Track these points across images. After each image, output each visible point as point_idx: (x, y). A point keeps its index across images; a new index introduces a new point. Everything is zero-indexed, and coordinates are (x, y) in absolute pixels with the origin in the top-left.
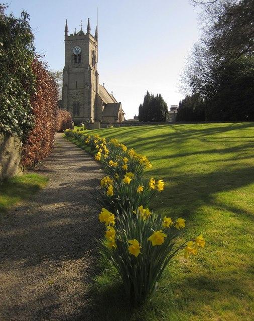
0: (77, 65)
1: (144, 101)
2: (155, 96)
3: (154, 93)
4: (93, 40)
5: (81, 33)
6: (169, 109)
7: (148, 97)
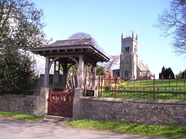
1: (162, 71)
3: (167, 67)
4: (136, 40)
7: (163, 68)
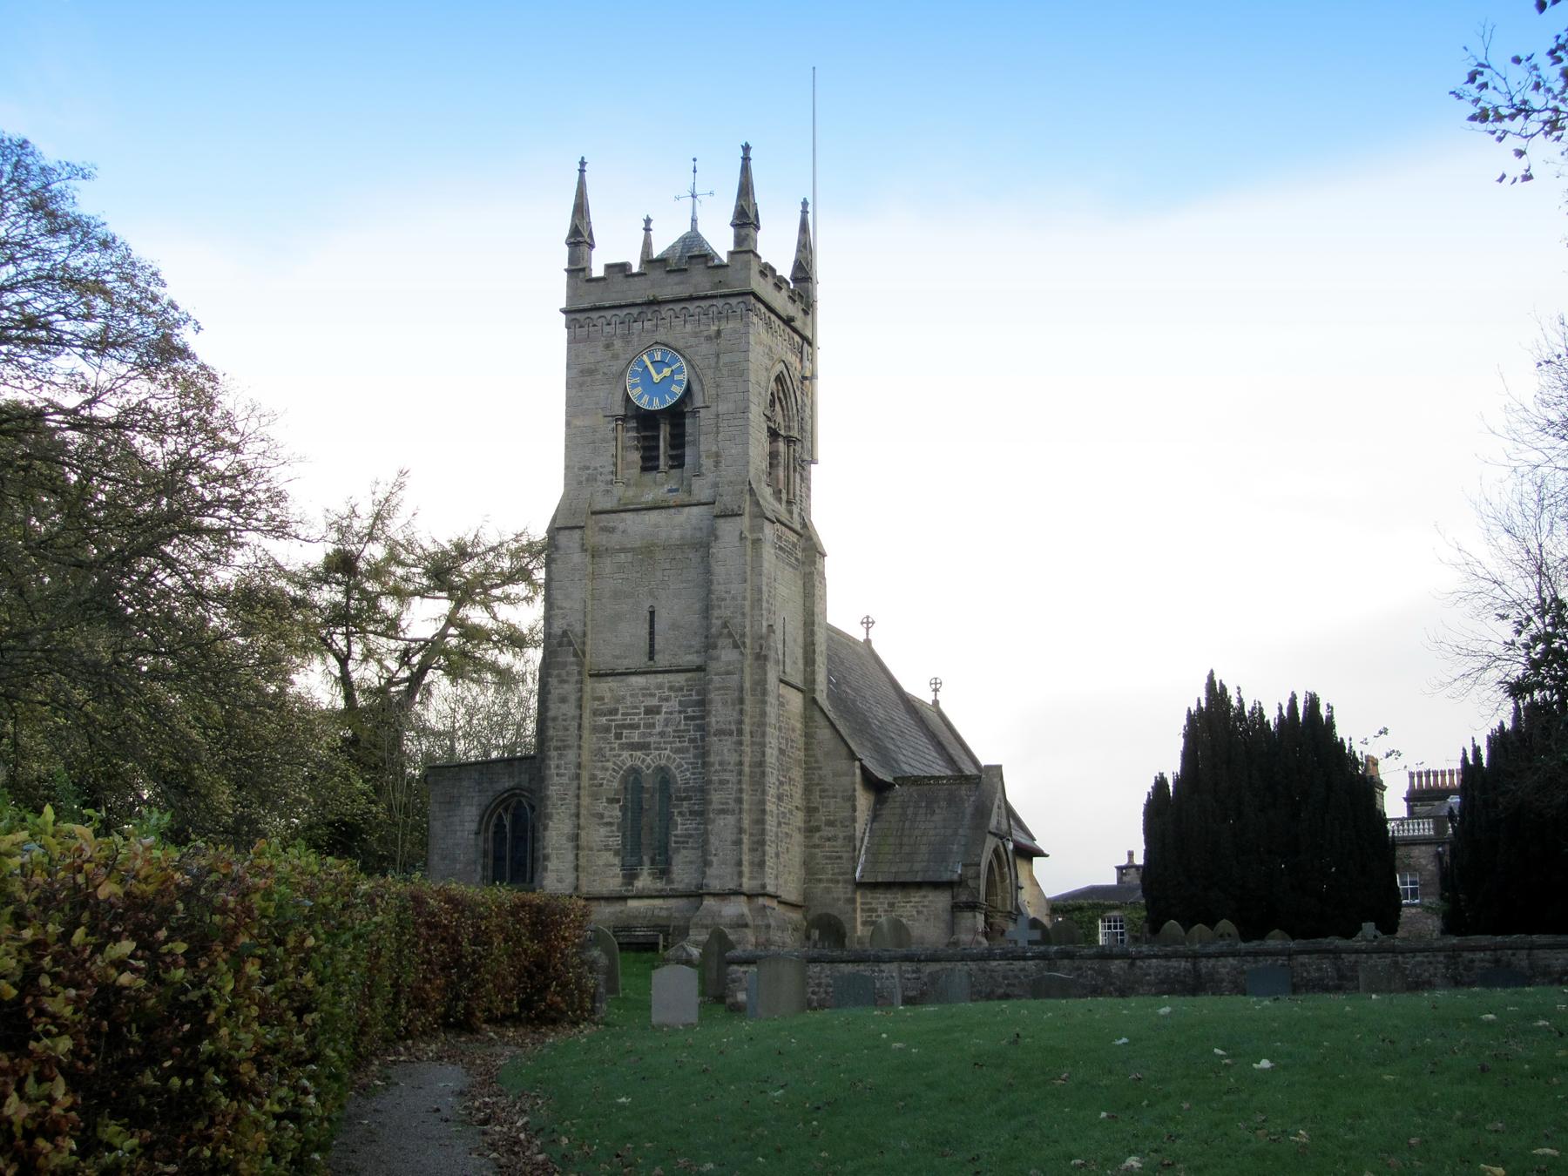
0: (658, 488)
2: (1271, 716)
3: (1266, 693)
5: (693, 253)
6: (1394, 805)
7: (1217, 727)
